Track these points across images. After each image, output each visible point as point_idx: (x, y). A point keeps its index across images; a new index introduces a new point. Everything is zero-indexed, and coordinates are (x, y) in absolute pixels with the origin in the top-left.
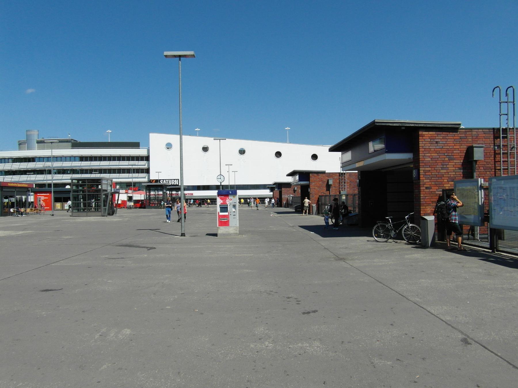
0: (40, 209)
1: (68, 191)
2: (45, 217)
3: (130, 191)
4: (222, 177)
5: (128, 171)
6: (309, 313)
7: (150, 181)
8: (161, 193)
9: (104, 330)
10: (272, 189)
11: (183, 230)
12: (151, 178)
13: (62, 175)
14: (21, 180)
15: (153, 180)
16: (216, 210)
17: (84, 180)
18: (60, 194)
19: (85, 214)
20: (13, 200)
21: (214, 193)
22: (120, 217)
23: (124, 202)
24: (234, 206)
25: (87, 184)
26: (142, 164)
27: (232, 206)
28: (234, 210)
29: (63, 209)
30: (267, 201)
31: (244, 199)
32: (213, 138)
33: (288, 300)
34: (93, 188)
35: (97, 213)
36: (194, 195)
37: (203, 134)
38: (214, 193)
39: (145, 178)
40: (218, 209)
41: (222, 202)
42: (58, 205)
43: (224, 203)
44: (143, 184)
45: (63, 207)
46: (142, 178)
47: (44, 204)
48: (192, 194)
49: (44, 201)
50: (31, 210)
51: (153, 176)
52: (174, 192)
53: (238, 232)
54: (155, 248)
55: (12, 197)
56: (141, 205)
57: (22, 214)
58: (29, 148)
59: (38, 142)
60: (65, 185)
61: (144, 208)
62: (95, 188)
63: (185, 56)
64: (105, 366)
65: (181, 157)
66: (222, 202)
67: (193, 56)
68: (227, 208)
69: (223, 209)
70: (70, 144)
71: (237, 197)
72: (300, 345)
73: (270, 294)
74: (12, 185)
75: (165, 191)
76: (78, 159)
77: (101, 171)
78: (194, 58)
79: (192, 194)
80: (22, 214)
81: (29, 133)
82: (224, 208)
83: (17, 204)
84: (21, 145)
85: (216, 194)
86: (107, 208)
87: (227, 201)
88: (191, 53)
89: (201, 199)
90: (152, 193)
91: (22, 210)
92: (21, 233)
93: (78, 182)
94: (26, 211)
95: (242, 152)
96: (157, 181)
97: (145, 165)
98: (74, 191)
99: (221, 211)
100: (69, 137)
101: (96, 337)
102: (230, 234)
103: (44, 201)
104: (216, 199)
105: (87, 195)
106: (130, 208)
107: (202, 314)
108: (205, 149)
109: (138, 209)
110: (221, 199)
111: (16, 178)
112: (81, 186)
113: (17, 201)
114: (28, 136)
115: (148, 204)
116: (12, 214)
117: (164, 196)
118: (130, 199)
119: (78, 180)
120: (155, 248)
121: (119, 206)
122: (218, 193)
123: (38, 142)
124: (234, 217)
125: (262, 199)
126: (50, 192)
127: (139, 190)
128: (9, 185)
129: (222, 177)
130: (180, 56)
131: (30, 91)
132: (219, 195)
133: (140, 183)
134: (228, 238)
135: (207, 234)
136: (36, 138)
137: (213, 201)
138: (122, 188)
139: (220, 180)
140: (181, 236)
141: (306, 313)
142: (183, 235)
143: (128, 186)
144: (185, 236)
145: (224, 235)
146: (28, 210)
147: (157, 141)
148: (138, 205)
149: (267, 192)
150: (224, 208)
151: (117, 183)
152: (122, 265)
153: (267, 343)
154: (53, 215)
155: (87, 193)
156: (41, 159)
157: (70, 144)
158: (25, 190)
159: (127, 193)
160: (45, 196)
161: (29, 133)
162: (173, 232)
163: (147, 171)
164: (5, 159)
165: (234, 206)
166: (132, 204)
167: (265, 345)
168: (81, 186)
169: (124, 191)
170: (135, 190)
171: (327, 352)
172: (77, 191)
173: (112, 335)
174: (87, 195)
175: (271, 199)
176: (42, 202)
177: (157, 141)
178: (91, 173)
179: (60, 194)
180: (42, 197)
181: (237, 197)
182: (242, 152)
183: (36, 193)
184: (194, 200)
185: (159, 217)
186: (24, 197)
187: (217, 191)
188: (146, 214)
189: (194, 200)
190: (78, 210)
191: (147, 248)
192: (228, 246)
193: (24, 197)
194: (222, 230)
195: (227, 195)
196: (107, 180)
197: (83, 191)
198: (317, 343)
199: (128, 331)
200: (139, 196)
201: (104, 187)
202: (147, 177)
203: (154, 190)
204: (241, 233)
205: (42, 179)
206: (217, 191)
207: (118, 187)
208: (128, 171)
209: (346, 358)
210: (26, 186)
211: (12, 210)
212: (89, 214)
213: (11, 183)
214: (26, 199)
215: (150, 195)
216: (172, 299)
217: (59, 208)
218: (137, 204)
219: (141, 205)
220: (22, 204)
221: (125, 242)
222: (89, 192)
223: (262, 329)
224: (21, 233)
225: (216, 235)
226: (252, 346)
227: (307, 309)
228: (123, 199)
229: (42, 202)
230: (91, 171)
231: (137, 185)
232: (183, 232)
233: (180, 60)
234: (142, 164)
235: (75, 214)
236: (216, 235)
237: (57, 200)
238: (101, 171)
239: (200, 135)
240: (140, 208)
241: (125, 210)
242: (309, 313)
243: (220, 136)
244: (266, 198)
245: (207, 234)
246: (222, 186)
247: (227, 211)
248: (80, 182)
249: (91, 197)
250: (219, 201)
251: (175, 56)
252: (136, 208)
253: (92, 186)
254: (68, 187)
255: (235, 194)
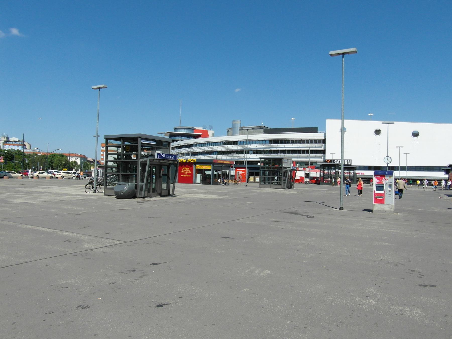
0: (238, 180)
1: (258, 168)
2: (241, 187)
3: (307, 169)
4: (389, 159)
5: (307, 152)
6: (426, 286)
7: (326, 161)
8: (334, 171)
9: (252, 268)
10: (447, 172)
11: (341, 204)
12: (327, 158)
13: (255, 155)
14: (228, 158)
15: (328, 161)
16: (372, 189)
17: (269, 159)
18: (253, 170)
19: (269, 186)
20: (220, 173)
21: (370, 173)
22: (297, 190)
23: (302, 178)
24: (390, 186)
25: (271, 162)
26: (319, 147)
27: (388, 186)
28: (389, 189)
29: (254, 181)
30: (443, 183)
31: (419, 180)
32: (381, 122)
33: (412, 272)
34: (276, 166)
35: (278, 186)
36: (365, 174)
37: (374, 118)
38: (370, 173)
39: (321, 158)
40: (375, 188)
41: (378, 181)
42: (251, 178)
43: (380, 183)
44: (318, 163)
45: (255, 180)
46: (318, 158)
47: (241, 177)
48: (363, 174)
49: (242, 174)
50: (232, 181)
51: (329, 157)
52: (352, 172)
53: (393, 210)
54: (313, 217)
55: (220, 171)
56: (316, 181)
57: (226, 184)
58: (234, 134)
59: (241, 129)
60: (257, 162)
61: (319, 184)
62: (277, 166)
63: (348, 53)
64: (245, 290)
65: (355, 141)
66: (378, 181)
67: (355, 52)
68: (383, 187)
69: (379, 188)
70: (263, 130)
71: (393, 178)
72: (401, 308)
73: (396, 265)
74: (222, 162)
75: (337, 170)
76: (268, 142)
77: (285, 152)
78: (356, 54)
79: (363, 174)
80: (226, 184)
81: (234, 123)
82: (380, 187)
83: (223, 176)
84: (229, 132)
85: (373, 174)
86: (286, 182)
87: (383, 180)
88: (354, 49)
89: (412, 180)
90: (326, 171)
91: (226, 181)
92: (222, 197)
93: (265, 161)
94: (228, 181)
95: (416, 134)
96: (331, 161)
97: (321, 147)
98: (262, 168)
99: (377, 190)
100: (262, 125)
101: (246, 271)
102: (385, 212)
103: (242, 174)
104: (372, 178)
105: (271, 171)
106: (306, 183)
107: (328, 270)
108: (378, 132)
109: (313, 185)
110: (377, 178)
111: (224, 157)
112: (267, 163)
113: (223, 173)
114: (234, 125)
115: (322, 180)
116: (219, 183)
117: (335, 174)
118: (307, 175)
119: (265, 159)
120: (313, 217)
121: (297, 181)
122: (375, 173)
123: (241, 129)
124: (390, 196)
125: (439, 181)
126: (245, 168)
127: (316, 168)
128: (219, 162)
129: (389, 158)
130: (343, 54)
131: (237, 90)
132: (375, 175)
133: (316, 162)
134: (382, 215)
135: (365, 210)
136: (238, 126)
137: (368, 180)
138: (301, 166)
139: (388, 162)
140: (340, 209)
141: (423, 286)
142: (341, 208)
143: (306, 164)
144: (343, 209)
145: (379, 211)
146: (230, 181)
147: (332, 127)
148: (314, 181)
149: (442, 175)
150: (380, 187)
151: (297, 162)
152: (283, 227)
153: (371, 300)
154: (246, 186)
155: (271, 170)
156: (242, 142)
157: (263, 130)
158: (228, 166)
159: (304, 170)
160: (243, 171)
161: (234, 123)
162: (335, 206)
163: (323, 152)
164: (205, 143)
165: (390, 186)
166: (308, 180)
167: (369, 301)
168: (267, 163)
169: (302, 169)
170: (312, 169)
171: (424, 319)
172: (264, 168)
173: (256, 272)
174: (271, 171)
175: (446, 181)
176: (240, 176)
177: (332, 127)
178: (277, 153)
179: (253, 170)
180: (240, 172)
181: (393, 178)
182: (416, 134)
183: (236, 168)
184: (428, 180)
185: (329, 192)
186: (227, 171)
187: (374, 171)
188: (319, 189)
189: (428, 180)
190: (265, 183)
191: (307, 216)
192: (379, 222)
193: (227, 171)
194: (377, 207)
195: (383, 175)
196: (287, 159)
197: (268, 168)
198: (419, 311)
199: (268, 272)
200: (315, 174)
201: (284, 165)
202: (323, 157)
203: (328, 169)
204: (396, 211)
205: (242, 157)
206: (374, 171)
207: (298, 165)
208: (307, 152)
209: (441, 327)
210: (229, 162)
211: (219, 180)
212: (272, 186)
213: (221, 160)
214: (229, 172)
215: (324, 173)
216: (309, 256)
217: (252, 180)
218: (312, 181)
219: (316, 181)
220: (227, 176)
221: (293, 210)
222: (273, 168)
223: (373, 290)
224: (222, 197)
225: (371, 211)
226: (357, 300)
227: (426, 283)
228: (301, 176)
229: (240, 176)
230: (277, 152)
231: (314, 164)
232: (341, 206)
233: (343, 57)
234: (319, 147)
235: (261, 186)
236: (371, 211)
237: (251, 174)
238: (285, 152)
239: (373, 120)
240: (315, 184)
241: (302, 185)
242: (426, 286)
243: (390, 118)
244: (417, 180)
245: (365, 210)
246: (389, 167)
247: (383, 190)
248: (267, 161)
249: (274, 173)
250: (375, 181)
251: (339, 54)
252: (311, 183)
253: (275, 164)
254: (259, 164)
255: (391, 174)
